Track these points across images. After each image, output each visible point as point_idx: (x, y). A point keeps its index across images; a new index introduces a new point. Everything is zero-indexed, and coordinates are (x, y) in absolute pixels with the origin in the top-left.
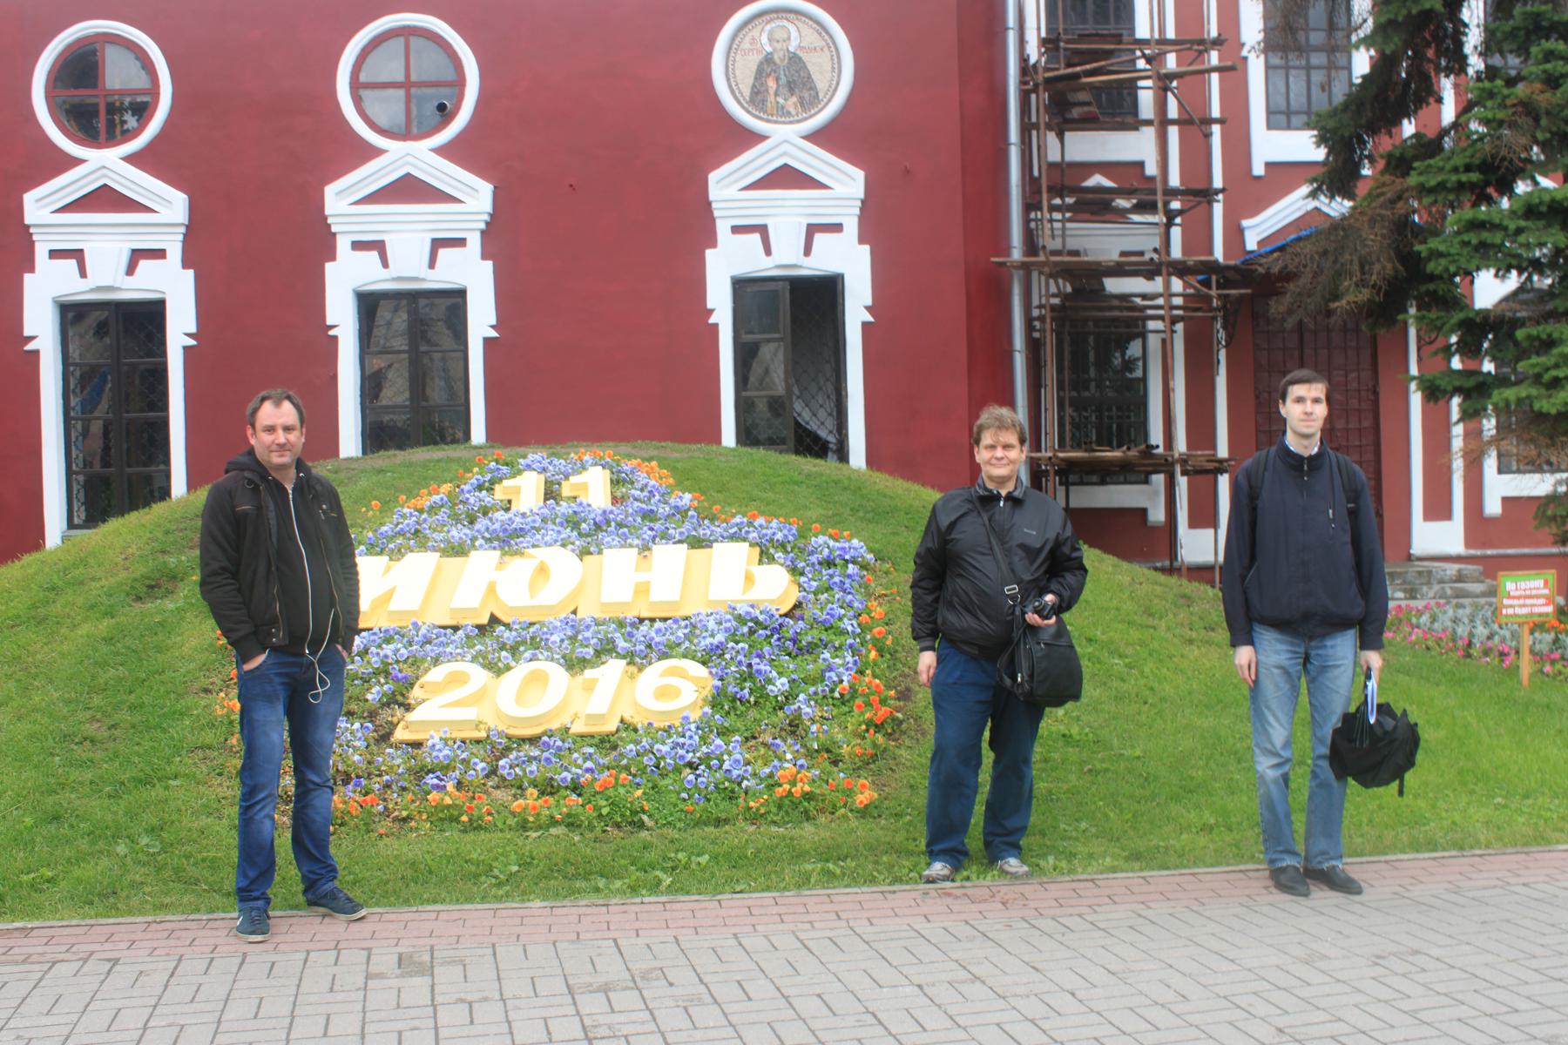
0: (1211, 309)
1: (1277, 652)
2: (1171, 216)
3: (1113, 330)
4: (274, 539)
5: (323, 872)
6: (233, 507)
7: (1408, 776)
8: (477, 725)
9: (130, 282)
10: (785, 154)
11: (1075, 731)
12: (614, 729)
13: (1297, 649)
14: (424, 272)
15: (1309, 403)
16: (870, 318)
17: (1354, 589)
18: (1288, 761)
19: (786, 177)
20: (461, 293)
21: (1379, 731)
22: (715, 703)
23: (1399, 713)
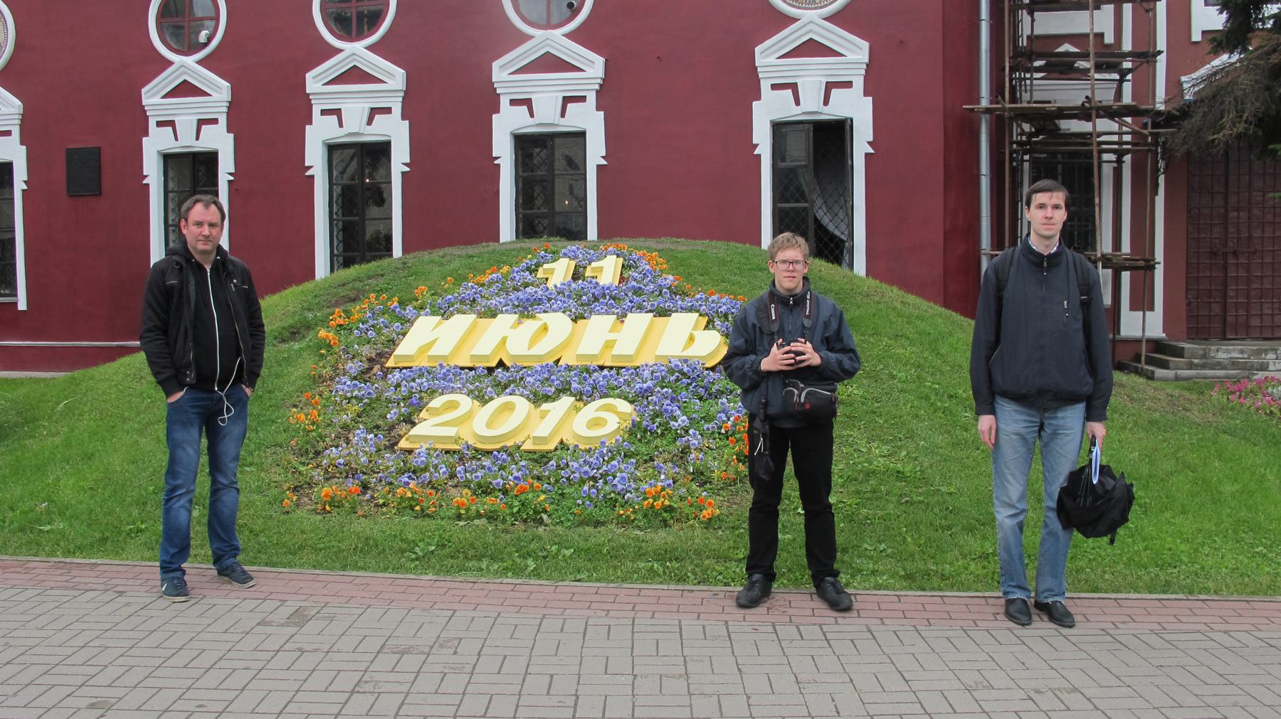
0: (1146, 144)
1: (1016, 422)
2: (1123, 74)
3: (1076, 160)
4: (193, 305)
5: (227, 549)
6: (164, 282)
7: (1121, 531)
8: (457, 440)
9: (370, 130)
10: (810, 31)
11: (908, 468)
12: (552, 448)
13: (1034, 419)
14: (556, 118)
15: (1049, 209)
16: (25, 187)
17: (1083, 370)
18: (1023, 511)
19: (811, 48)
20: (582, 134)
21: (1100, 491)
22: (631, 432)
23: (1118, 476)
